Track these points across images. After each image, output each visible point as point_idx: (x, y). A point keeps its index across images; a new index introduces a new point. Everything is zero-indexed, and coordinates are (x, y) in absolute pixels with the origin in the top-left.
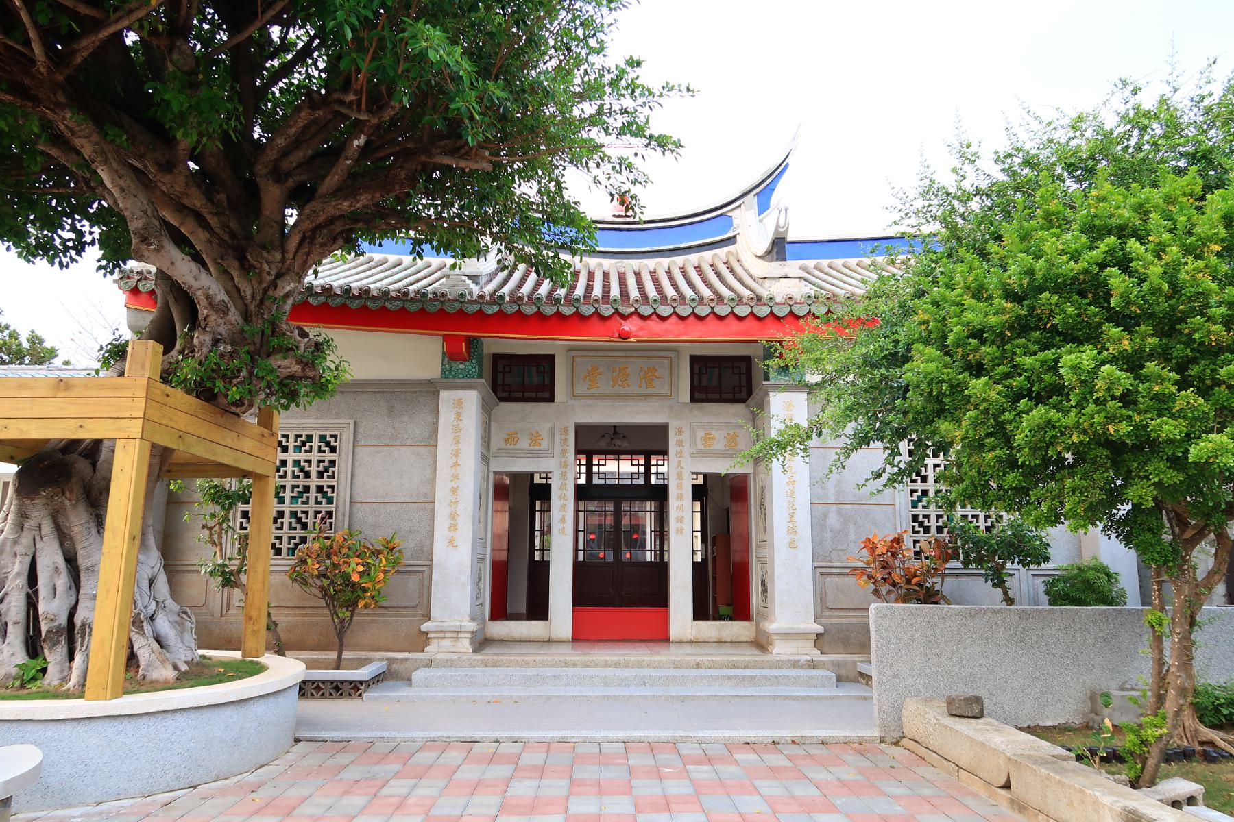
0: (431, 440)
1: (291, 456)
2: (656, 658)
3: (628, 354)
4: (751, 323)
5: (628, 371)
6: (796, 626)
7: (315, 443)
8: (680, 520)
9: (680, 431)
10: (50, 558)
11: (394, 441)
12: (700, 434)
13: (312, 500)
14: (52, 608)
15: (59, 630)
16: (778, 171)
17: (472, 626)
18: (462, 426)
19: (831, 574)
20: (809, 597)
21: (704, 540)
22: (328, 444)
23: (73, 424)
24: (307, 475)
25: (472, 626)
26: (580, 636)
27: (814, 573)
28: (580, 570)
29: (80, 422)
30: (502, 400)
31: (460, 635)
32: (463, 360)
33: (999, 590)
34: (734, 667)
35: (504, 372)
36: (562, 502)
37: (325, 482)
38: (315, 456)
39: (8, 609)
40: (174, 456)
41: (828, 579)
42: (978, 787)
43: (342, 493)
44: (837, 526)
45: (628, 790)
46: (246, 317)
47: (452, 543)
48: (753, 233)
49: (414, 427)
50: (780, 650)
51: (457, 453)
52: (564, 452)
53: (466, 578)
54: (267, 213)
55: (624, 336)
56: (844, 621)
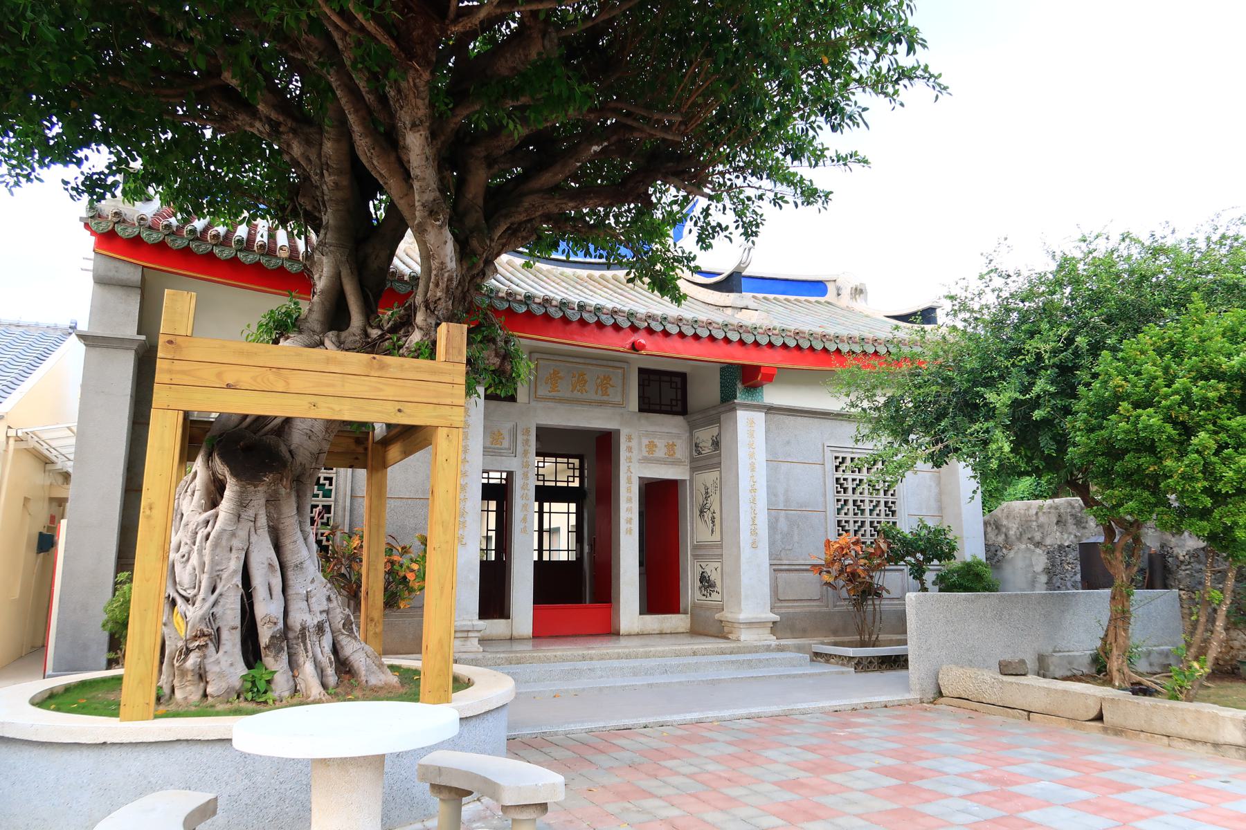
3: (588, 361)
9: (629, 438)
10: (263, 554)
12: (645, 441)
14: (267, 609)
20: (766, 590)
21: (579, 540)
23: (391, 407)
26: (543, 631)
29: (314, 399)
31: (471, 634)
34: (723, 653)
35: (671, 382)
39: (224, 613)
40: (297, 437)
41: (779, 575)
44: (785, 529)
50: (747, 637)
51: (465, 451)
52: (526, 453)
54: (470, 196)
56: (791, 610)
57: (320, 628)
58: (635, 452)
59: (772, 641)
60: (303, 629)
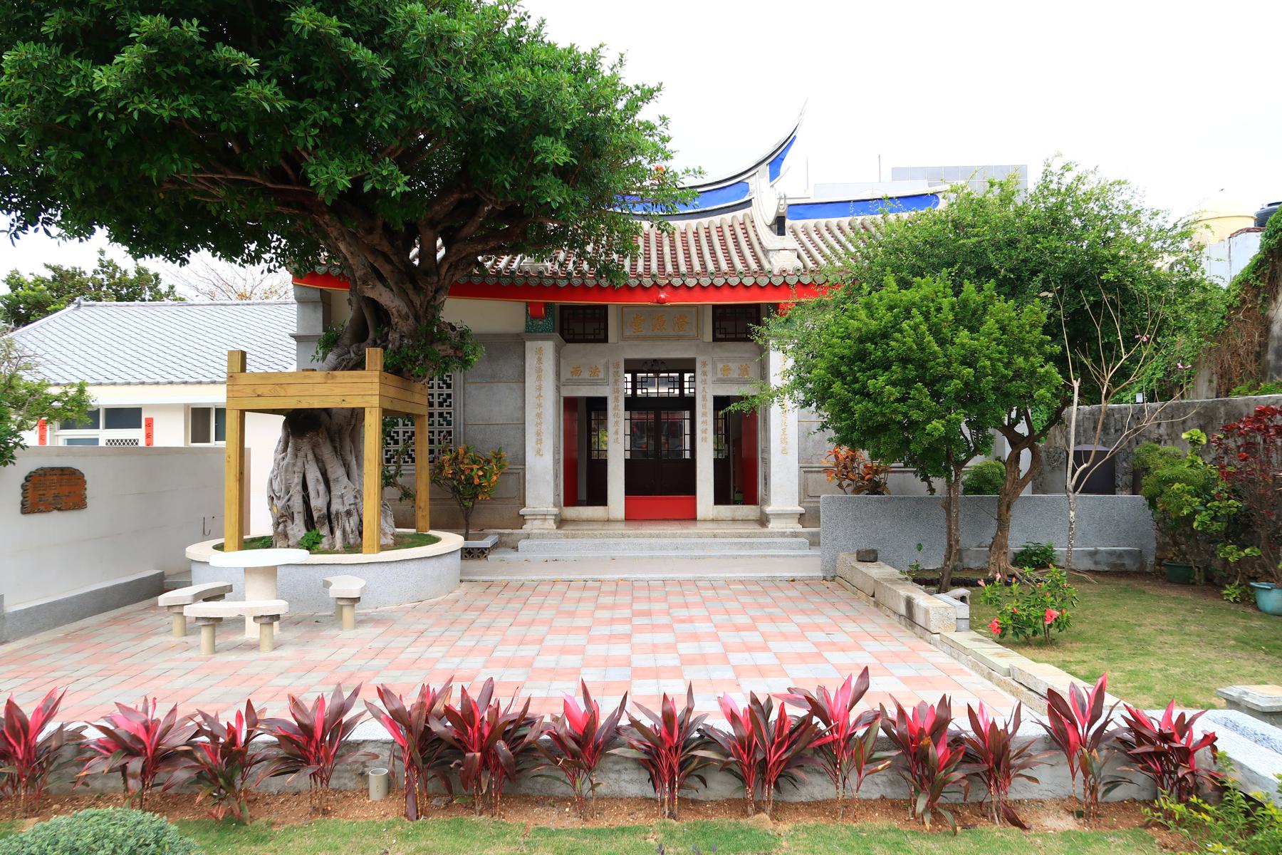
0: (521, 378)
2: (685, 531)
4: (755, 290)
9: (704, 364)
10: (313, 474)
11: (494, 379)
14: (318, 503)
16: (787, 143)
17: (556, 511)
23: (338, 399)
25: (556, 511)
30: (568, 341)
32: (541, 318)
33: (925, 484)
37: (445, 410)
38: (436, 391)
42: (863, 595)
43: (458, 417)
45: (665, 600)
46: (417, 318)
47: (539, 453)
48: (766, 199)
50: (774, 526)
51: (540, 388)
53: (550, 477)
55: (660, 301)
57: (349, 513)
59: (799, 528)
60: (337, 513)
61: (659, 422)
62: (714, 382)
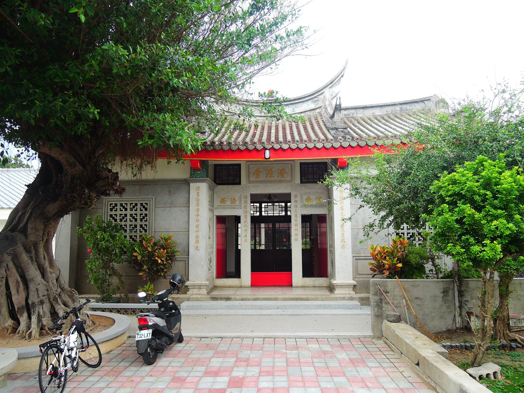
1: (129, 212)
5: (273, 170)
6: (344, 282)
7: (139, 206)
8: (296, 235)
9: (296, 196)
11: (172, 205)
12: (305, 197)
13: (138, 231)
14: (18, 299)
15: (23, 307)
16: (341, 75)
18: (200, 198)
19: (360, 259)
22: (144, 207)
24: (136, 220)
26: (255, 284)
27: (353, 259)
28: (255, 253)
30: (218, 184)
32: (199, 170)
36: (245, 228)
37: (143, 223)
38: (138, 212)
41: (359, 261)
49: (180, 198)
50: (337, 291)
52: (246, 207)
56: (361, 279)
58: (299, 202)
61: (276, 230)
62: (302, 207)
